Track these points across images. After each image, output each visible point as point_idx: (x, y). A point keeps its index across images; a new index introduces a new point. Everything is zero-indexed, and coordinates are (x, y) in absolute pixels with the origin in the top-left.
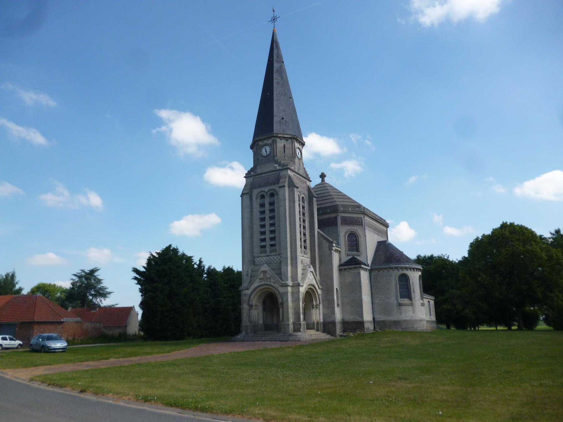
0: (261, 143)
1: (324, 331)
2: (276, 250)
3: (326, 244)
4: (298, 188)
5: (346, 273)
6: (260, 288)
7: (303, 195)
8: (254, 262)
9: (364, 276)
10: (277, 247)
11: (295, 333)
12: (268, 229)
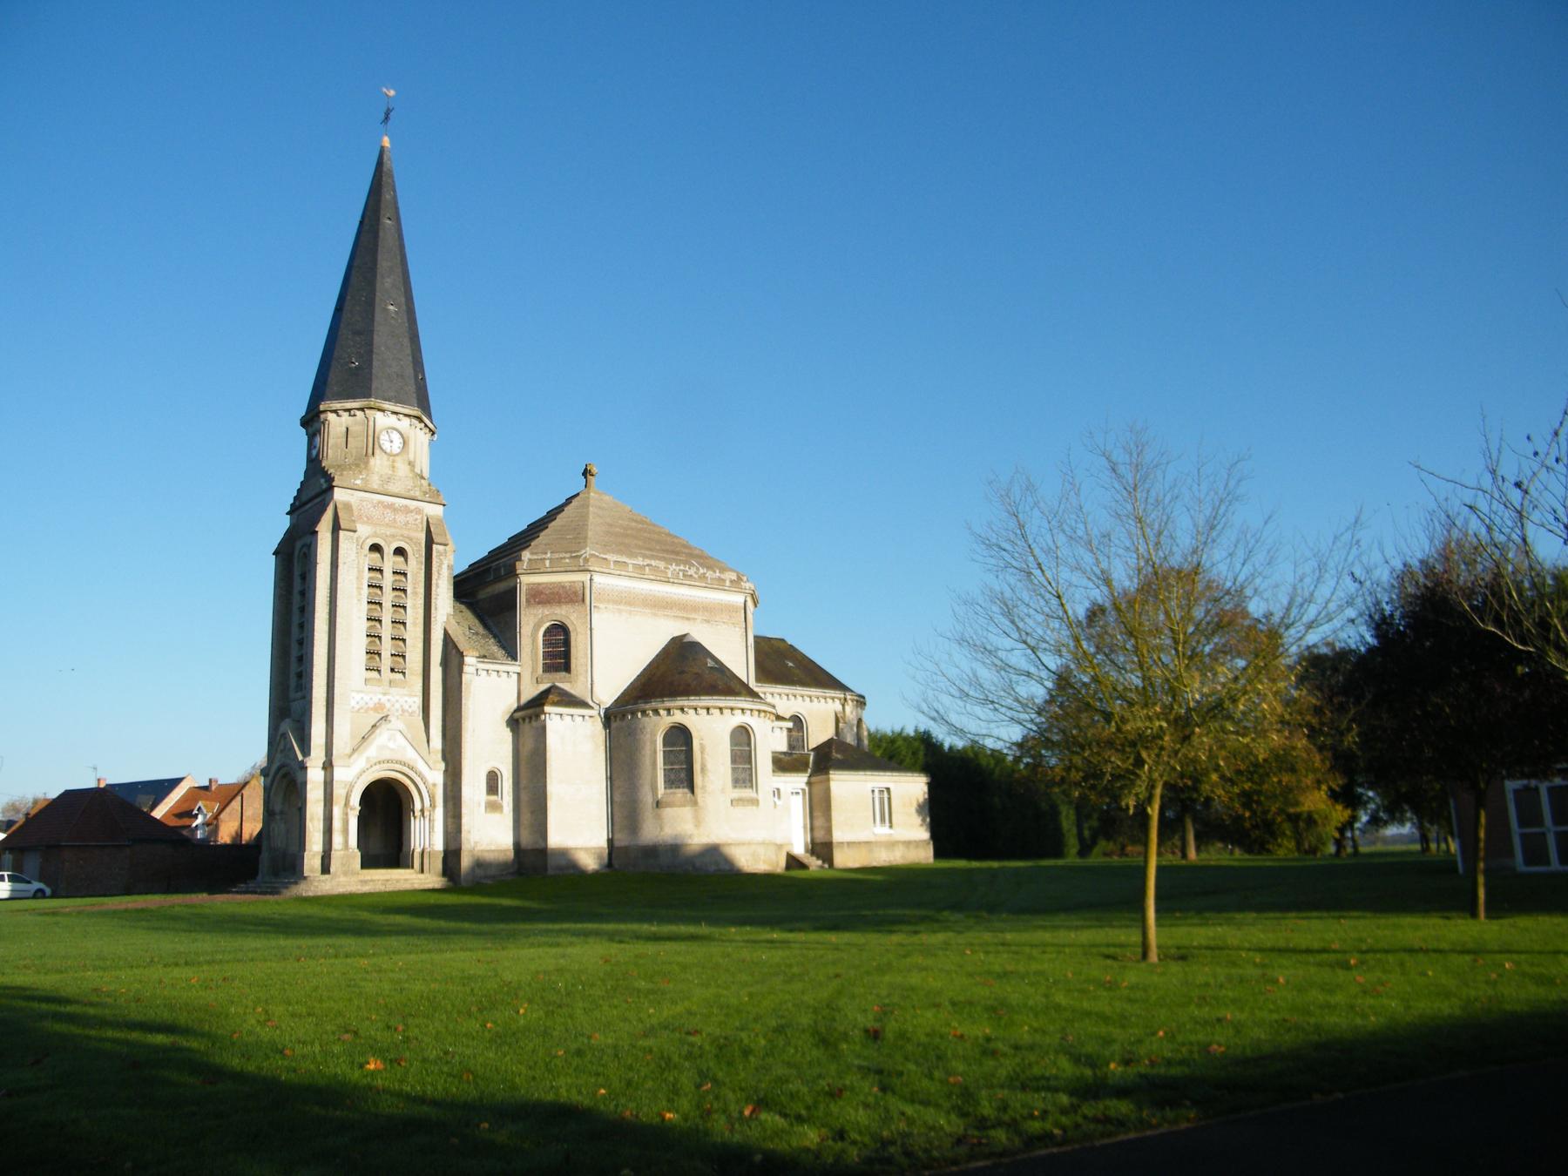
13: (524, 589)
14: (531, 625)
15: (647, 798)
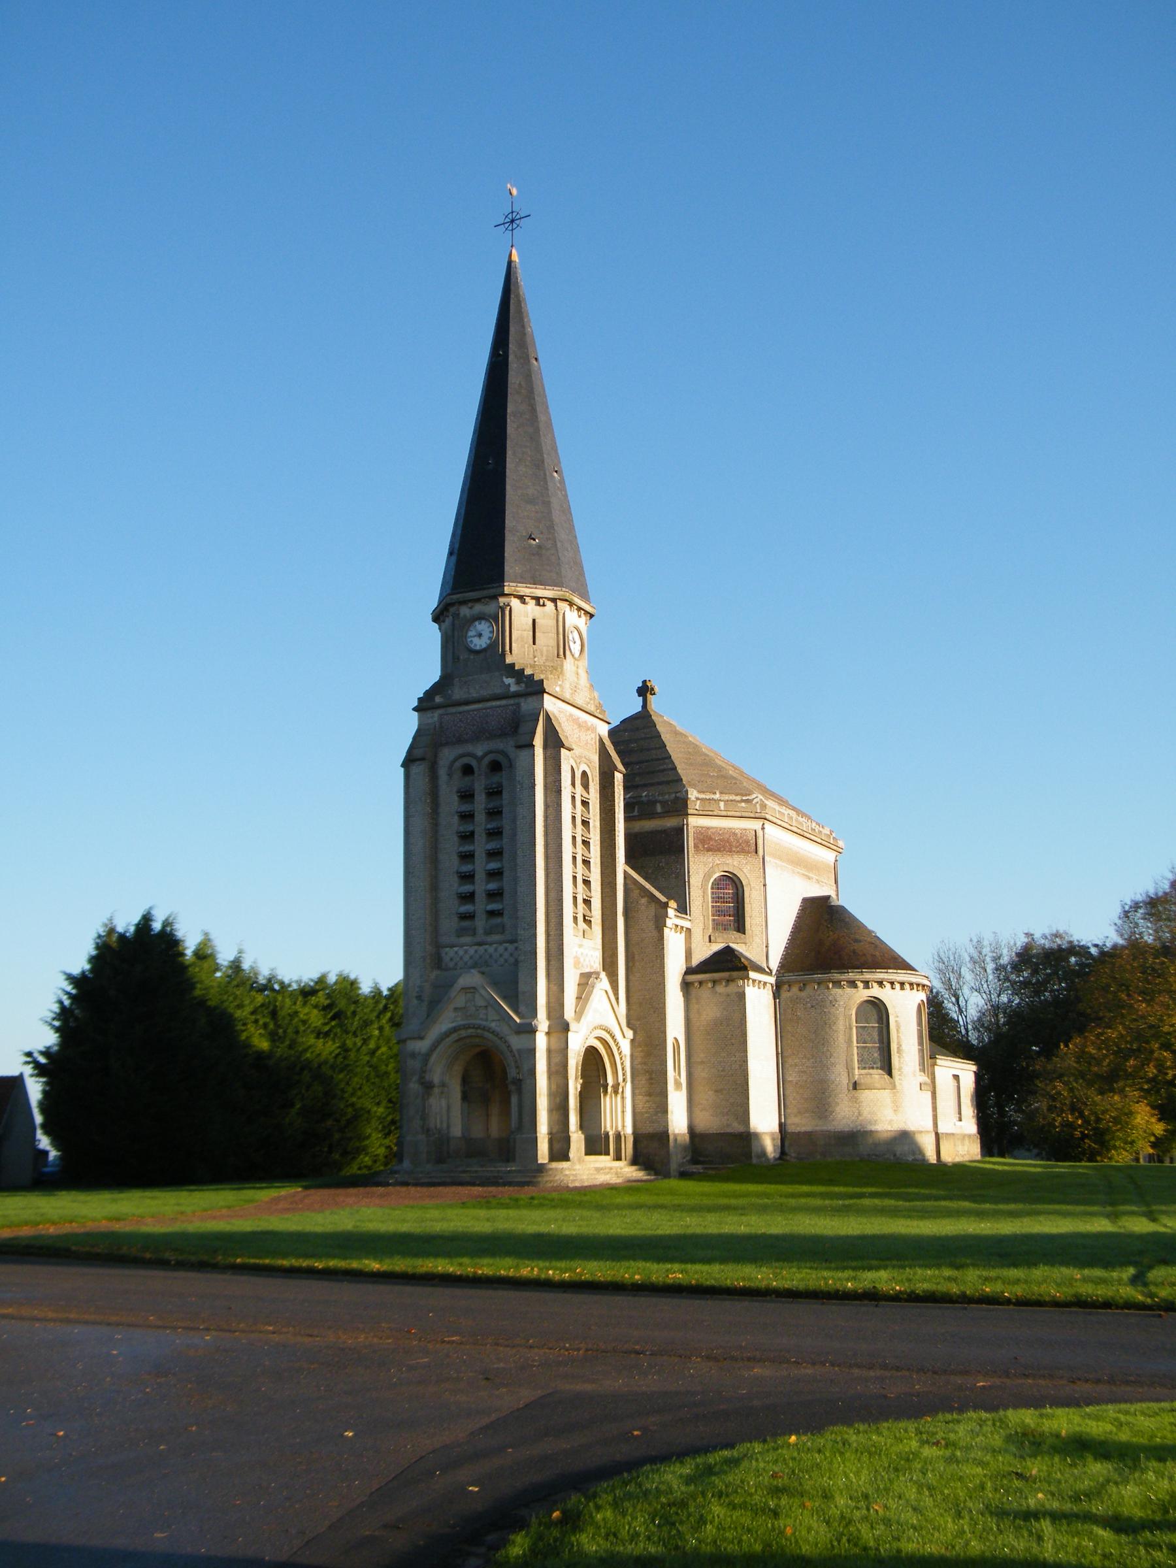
0: (465, 611)
1: (634, 1162)
2: (503, 927)
3: (646, 912)
4: (569, 750)
5: (705, 993)
6: (455, 1036)
7: (583, 767)
9: (759, 1002)
10: (506, 919)
11: (554, 1165)
12: (481, 865)
13: (691, 831)
14: (701, 871)
15: (841, 1079)
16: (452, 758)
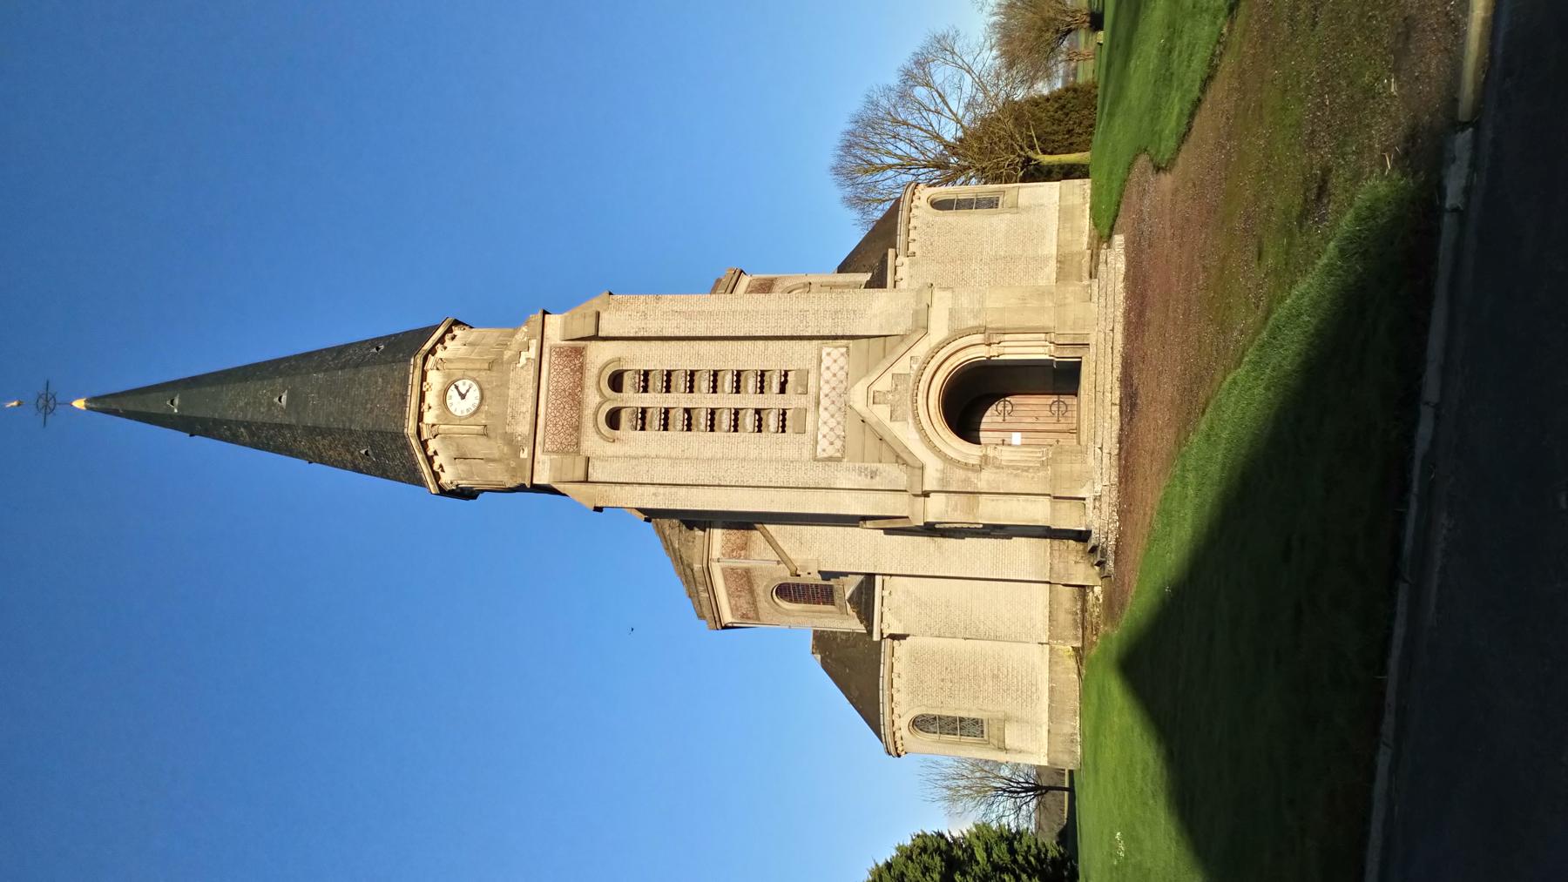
8: (830, 459)
12: (726, 400)
16: (596, 437)
